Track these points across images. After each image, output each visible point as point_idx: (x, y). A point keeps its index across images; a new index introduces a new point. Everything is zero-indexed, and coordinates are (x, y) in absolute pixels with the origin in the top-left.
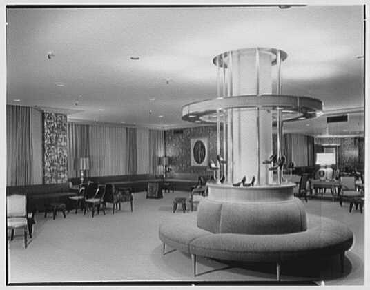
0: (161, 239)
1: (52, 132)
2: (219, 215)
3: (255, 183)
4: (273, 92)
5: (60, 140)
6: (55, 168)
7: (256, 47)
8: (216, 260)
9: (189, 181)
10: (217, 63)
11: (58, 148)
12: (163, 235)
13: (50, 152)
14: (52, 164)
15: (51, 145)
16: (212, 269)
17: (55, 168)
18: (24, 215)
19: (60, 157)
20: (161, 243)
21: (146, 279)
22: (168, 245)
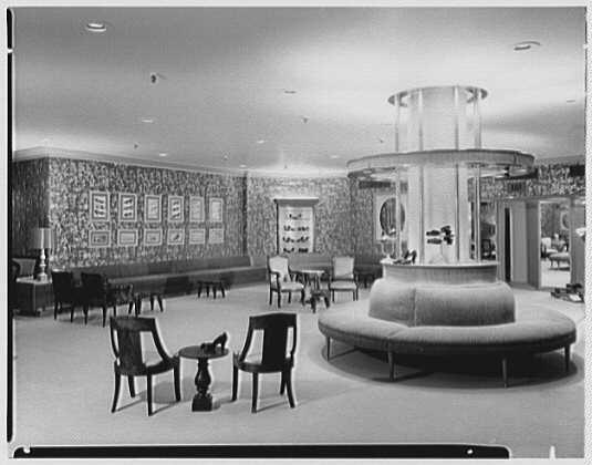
0: (324, 333)
1: (71, 191)
2: (413, 299)
3: (417, 259)
4: (476, 145)
5: (82, 201)
6: (75, 246)
7: (455, 84)
8: (364, 351)
9: (219, 271)
10: (396, 102)
11: (80, 213)
12: (327, 327)
13: (100, 174)
14: (71, 240)
15: (69, 210)
16: (415, 371)
17: (75, 246)
18: (311, 209)
19: (83, 227)
20: (324, 338)
21: (461, 441)
22: (335, 339)
